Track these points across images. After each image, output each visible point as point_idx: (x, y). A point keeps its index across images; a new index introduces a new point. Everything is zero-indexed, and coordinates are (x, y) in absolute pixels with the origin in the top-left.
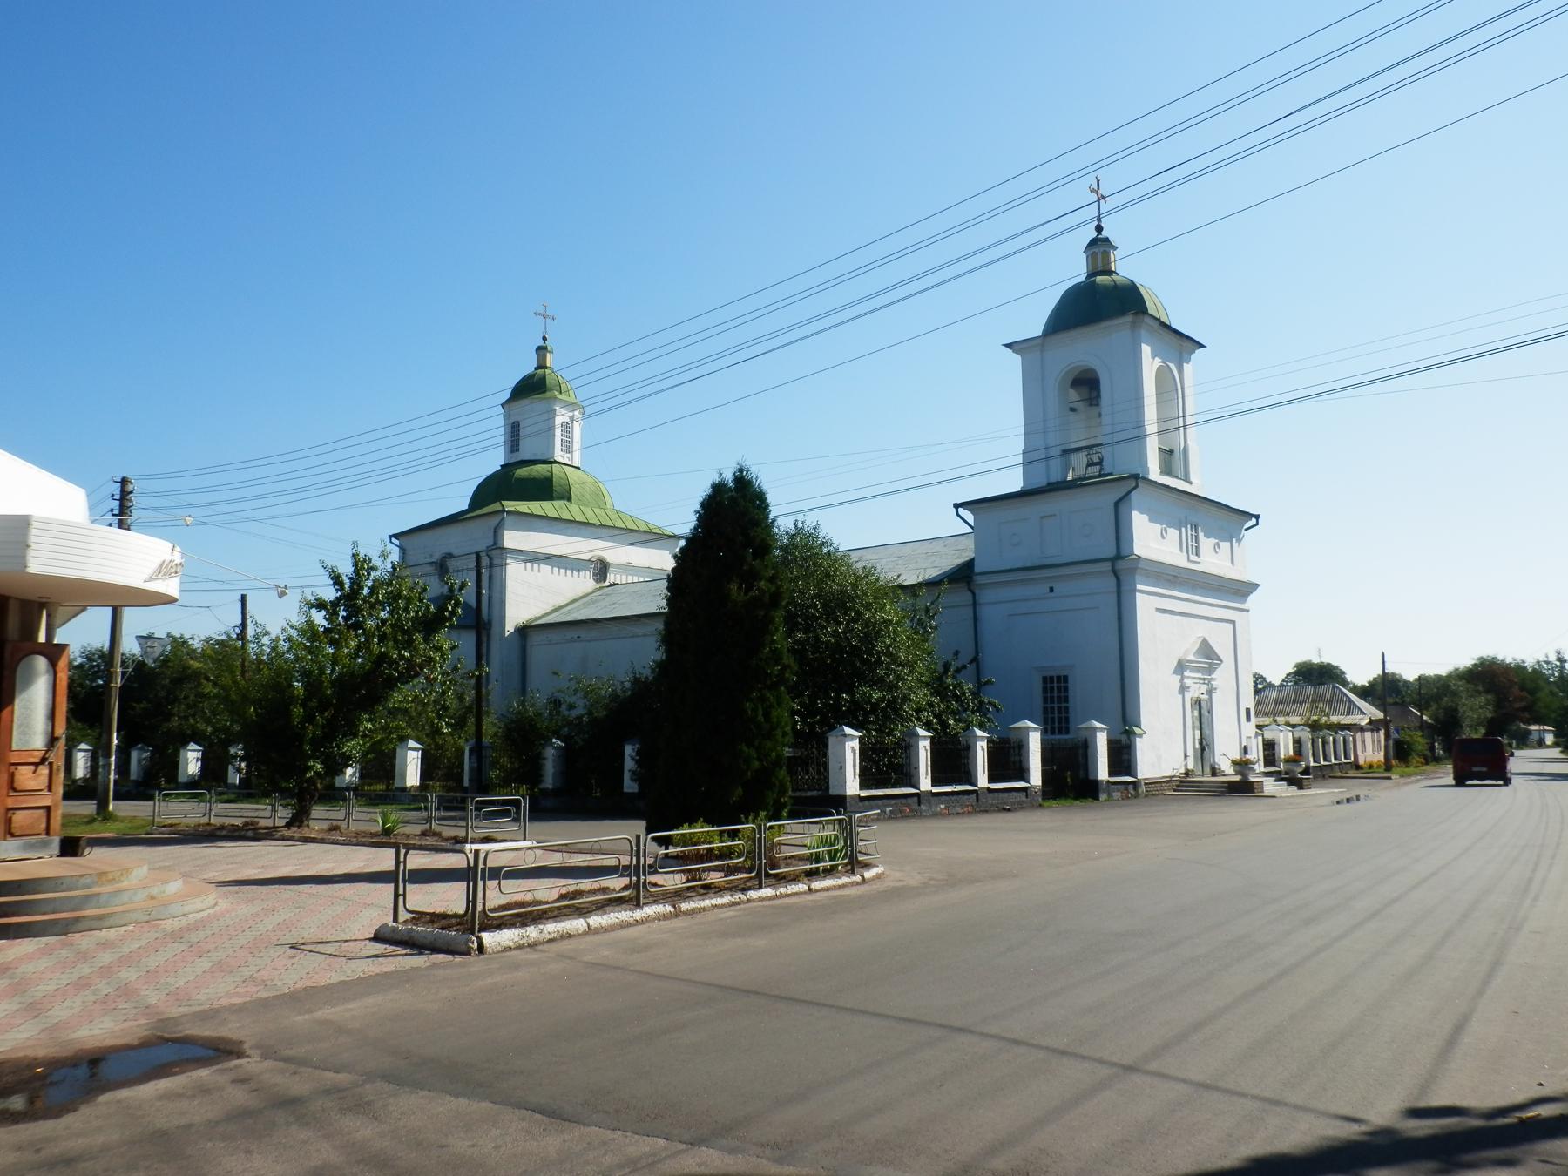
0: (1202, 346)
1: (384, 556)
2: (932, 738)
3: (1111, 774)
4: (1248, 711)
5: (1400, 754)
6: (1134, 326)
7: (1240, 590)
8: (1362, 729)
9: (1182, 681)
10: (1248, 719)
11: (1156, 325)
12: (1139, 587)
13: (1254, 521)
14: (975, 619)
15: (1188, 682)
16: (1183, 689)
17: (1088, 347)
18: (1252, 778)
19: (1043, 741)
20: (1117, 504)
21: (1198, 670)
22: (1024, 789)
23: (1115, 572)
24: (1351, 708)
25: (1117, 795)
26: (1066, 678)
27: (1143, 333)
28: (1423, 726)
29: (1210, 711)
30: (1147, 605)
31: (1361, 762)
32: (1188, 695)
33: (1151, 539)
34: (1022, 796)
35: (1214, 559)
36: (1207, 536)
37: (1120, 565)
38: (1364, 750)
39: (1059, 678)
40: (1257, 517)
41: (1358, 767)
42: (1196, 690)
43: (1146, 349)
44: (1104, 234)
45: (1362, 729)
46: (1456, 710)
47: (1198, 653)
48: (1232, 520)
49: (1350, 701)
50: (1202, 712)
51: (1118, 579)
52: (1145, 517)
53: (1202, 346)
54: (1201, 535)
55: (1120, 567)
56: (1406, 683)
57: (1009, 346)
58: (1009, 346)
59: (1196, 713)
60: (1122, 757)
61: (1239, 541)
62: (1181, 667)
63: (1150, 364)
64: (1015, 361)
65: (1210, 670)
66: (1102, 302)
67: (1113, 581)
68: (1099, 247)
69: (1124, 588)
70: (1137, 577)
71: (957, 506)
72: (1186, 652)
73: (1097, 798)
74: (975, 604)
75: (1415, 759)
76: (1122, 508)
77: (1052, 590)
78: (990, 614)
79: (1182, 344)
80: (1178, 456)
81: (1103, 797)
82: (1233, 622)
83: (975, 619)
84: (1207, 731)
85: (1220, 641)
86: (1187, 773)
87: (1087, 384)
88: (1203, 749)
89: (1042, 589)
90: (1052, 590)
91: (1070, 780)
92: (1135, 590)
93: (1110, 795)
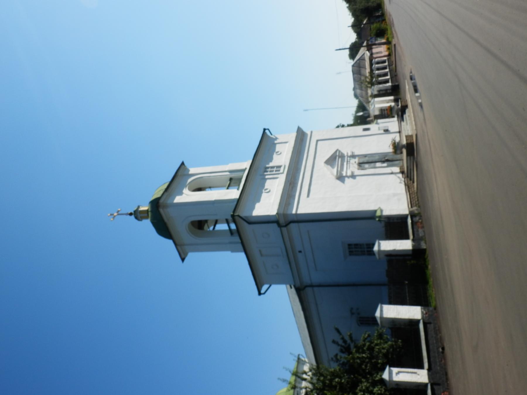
0: (183, 164)
1: (373, 2)
2: (390, 366)
3: (407, 238)
4: (365, 130)
5: (381, 33)
6: (166, 206)
7: (301, 137)
8: (372, 54)
9: (348, 177)
10: (368, 129)
11: (166, 194)
12: (294, 212)
13: (267, 131)
14: (320, 286)
15: (349, 174)
16: (353, 176)
17: (180, 225)
18: (404, 142)
19: (391, 302)
20: (250, 223)
21: (342, 165)
22: (425, 324)
23: (286, 226)
24: (362, 59)
25: (421, 234)
26: (349, 245)
27: (169, 202)
28: (369, 23)
29: (365, 156)
30: (305, 206)
31: (387, 53)
32: (357, 172)
33: (267, 206)
34: (431, 327)
35: (282, 157)
36: (271, 159)
37: (282, 221)
38: (381, 52)
39: (349, 248)
40: (265, 130)
41: (389, 55)
42: (352, 167)
43: (178, 199)
44: (133, 212)
45: (372, 54)
46: (362, 9)
47: (332, 166)
48: (266, 143)
49: (359, 59)
50: (367, 161)
51: (306, 286)
52: (257, 205)
53: (183, 164)
54: (271, 164)
55: (285, 222)
56: (354, 21)
57: (183, 260)
58: (183, 260)
59: (367, 166)
60: (395, 227)
61: (276, 139)
62: (341, 178)
63: (187, 196)
64: (191, 256)
65: (342, 156)
66: (158, 216)
67: (292, 225)
68: (138, 215)
69: (295, 219)
70: (289, 212)
71: (260, 294)
72: (332, 174)
73: (425, 250)
74: (312, 286)
75: (383, 26)
76: (253, 220)
77: (300, 252)
78: (316, 278)
79: (181, 173)
80: (234, 175)
81: (423, 246)
82: (317, 141)
83: (320, 286)
84: (377, 158)
85: (326, 151)
86: (402, 172)
87: (199, 225)
88: (387, 161)
89: (300, 256)
90: (300, 252)
91: (411, 277)
92: (296, 214)
93: (421, 239)
